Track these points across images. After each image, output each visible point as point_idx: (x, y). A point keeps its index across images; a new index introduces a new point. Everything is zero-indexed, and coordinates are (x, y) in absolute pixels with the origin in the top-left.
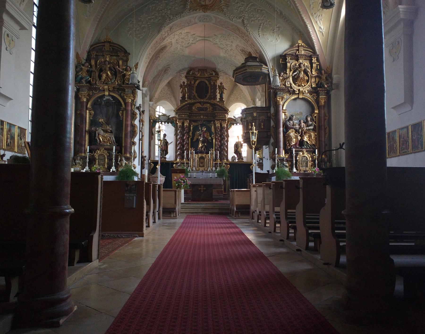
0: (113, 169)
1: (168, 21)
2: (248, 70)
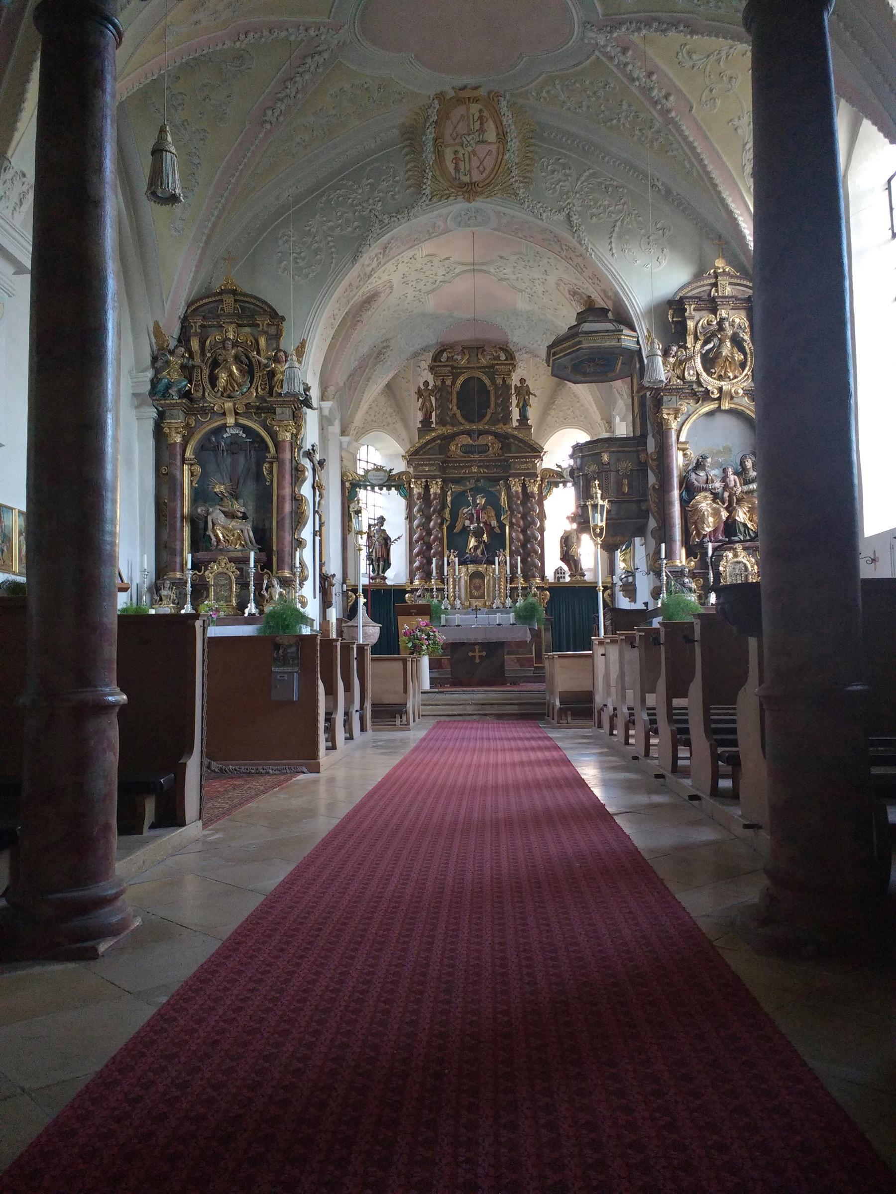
0: (251, 608)
1: (378, 231)
2: (585, 345)
